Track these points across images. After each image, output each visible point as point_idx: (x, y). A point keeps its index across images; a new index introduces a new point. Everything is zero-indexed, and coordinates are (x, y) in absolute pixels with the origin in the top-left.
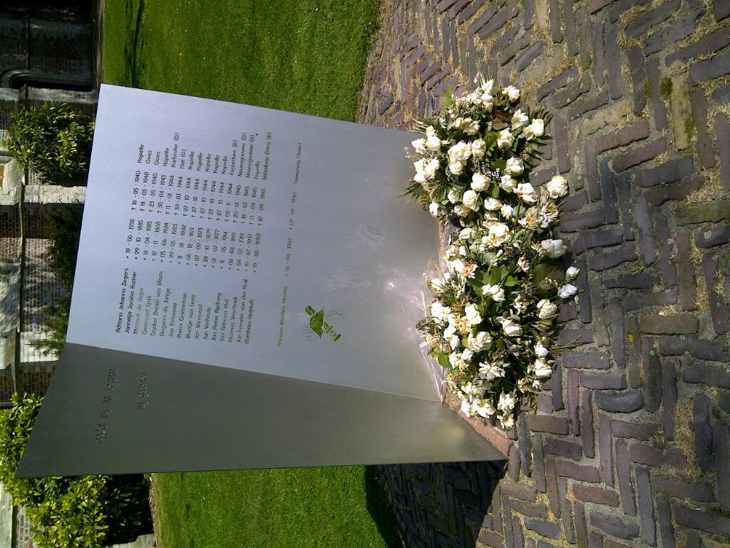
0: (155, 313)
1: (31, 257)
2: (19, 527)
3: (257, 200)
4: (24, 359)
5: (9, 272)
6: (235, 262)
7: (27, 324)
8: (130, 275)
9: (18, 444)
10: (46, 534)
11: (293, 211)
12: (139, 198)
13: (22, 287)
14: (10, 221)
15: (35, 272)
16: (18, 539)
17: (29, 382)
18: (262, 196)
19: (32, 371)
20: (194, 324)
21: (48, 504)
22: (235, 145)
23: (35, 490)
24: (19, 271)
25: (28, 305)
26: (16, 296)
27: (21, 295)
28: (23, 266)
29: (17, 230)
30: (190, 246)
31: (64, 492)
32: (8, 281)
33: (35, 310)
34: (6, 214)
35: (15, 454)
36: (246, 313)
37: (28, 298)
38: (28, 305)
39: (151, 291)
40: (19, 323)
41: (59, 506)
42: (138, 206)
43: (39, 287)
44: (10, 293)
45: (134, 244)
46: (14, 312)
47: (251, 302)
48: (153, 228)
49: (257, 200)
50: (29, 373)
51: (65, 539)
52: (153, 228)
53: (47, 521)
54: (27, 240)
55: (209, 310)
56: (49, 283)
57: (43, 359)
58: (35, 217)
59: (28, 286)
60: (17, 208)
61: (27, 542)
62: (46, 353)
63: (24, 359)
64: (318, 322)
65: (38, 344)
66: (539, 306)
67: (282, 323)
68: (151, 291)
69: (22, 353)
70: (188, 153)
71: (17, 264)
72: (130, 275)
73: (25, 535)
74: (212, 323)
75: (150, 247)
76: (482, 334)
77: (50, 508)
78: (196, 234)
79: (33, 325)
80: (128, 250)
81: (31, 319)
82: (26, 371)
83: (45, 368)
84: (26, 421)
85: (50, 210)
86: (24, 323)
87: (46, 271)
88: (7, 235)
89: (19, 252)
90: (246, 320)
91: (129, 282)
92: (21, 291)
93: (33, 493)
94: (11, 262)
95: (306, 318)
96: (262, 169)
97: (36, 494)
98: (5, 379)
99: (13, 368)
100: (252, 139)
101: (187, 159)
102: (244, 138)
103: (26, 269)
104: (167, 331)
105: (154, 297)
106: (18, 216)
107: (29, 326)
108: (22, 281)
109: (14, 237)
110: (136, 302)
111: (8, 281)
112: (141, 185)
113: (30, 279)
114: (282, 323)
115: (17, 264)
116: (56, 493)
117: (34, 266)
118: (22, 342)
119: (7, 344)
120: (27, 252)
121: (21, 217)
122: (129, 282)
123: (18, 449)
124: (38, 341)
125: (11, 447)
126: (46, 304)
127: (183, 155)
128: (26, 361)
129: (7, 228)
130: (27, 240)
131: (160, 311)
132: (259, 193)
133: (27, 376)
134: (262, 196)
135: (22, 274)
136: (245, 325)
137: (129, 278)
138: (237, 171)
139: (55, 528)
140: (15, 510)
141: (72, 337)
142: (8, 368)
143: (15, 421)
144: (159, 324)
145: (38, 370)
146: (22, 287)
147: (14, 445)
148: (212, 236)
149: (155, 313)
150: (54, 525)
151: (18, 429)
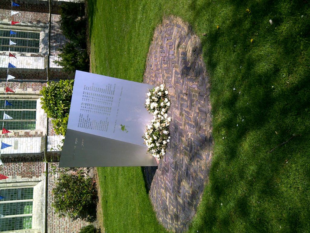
0: (87, 123)
1: (53, 22)
2: (49, 124)
3: (111, 100)
4: (51, 66)
5: (45, 28)
6: (105, 113)
7: (52, 50)
8: (81, 115)
9: (49, 99)
10: (58, 129)
11: (119, 103)
12: (82, 108)
13: (50, 35)
14: (45, 7)
15: (55, 29)
16: (49, 128)
17: (52, 74)
18: (112, 99)
19: (53, 71)
20: (95, 127)
21: (59, 120)
22: (107, 86)
23: (55, 114)
24: (49, 28)
25: (52, 43)
26: (47, 38)
27: (49, 38)
28: (50, 25)
29: (48, 10)
30: (95, 109)
31: (64, 116)
32: (45, 31)
33: (54, 44)
34: (44, 4)
35: (48, 102)
36: (107, 125)
37: (52, 39)
38: (52, 43)
39: (86, 119)
40: (49, 49)
41: (62, 121)
42: (83, 99)
43: (56, 36)
44: (45, 37)
45: (82, 108)
46: (47, 45)
47: (108, 122)
48: (87, 105)
49: (111, 100)
50: (53, 71)
51: (64, 132)
52: (87, 105)
53: (58, 125)
54: (52, 15)
55: (98, 124)
56: (60, 34)
57: (57, 67)
58: (54, 6)
59: (52, 35)
60: (48, 2)
61: (52, 129)
62: (58, 65)
63: (51, 66)
64: (123, 128)
65: (56, 62)
66: (163, 142)
67: (115, 128)
68: (86, 119)
69: (50, 64)
70: (97, 88)
71: (48, 25)
72: (81, 115)
73: (51, 127)
74: (99, 127)
75: (86, 109)
76: (152, 144)
77: (59, 121)
78: (96, 107)
79: (54, 51)
80: (81, 109)
81: (53, 48)
82: (52, 70)
83: (58, 70)
84: (52, 92)
85: (60, 3)
86: (50, 50)
87: (58, 28)
88: (44, 12)
89: (49, 20)
90: (106, 126)
91: (81, 116)
92: (49, 37)
93: (54, 115)
94: (46, 23)
95: (120, 127)
96: (113, 92)
97: (55, 116)
98: (44, 72)
99: (47, 69)
100: (111, 85)
101: (95, 89)
102: (109, 85)
103: (51, 27)
104: (89, 128)
105: (86, 120)
106: (48, 5)
107: (52, 51)
108: (50, 32)
109: (47, 13)
110: (82, 121)
111: (45, 31)
112: (84, 95)
113: (53, 31)
114: (115, 128)
115: (48, 25)
116: (61, 116)
117: (54, 26)
118: (50, 59)
119: (45, 60)
120: (52, 20)
121: (49, 5)
122: (81, 116)
123: (49, 101)
124: (56, 61)
125: (47, 99)
126: (58, 43)
127: (95, 88)
128: (51, 67)
129: (44, 9)
130: (52, 15)
131: (88, 123)
132: (112, 98)
133: (52, 72)
134: (112, 99)
135: (50, 29)
136: (106, 128)
137: (81, 116)
138: (109, 93)
139: (61, 128)
140: (48, 119)
141: (68, 128)
142: (45, 69)
143: (48, 91)
144: (87, 126)
145: (55, 70)
146: (50, 35)
147: (48, 99)
148: (100, 107)
149: (87, 123)
150: (60, 127)
151: (49, 94)
